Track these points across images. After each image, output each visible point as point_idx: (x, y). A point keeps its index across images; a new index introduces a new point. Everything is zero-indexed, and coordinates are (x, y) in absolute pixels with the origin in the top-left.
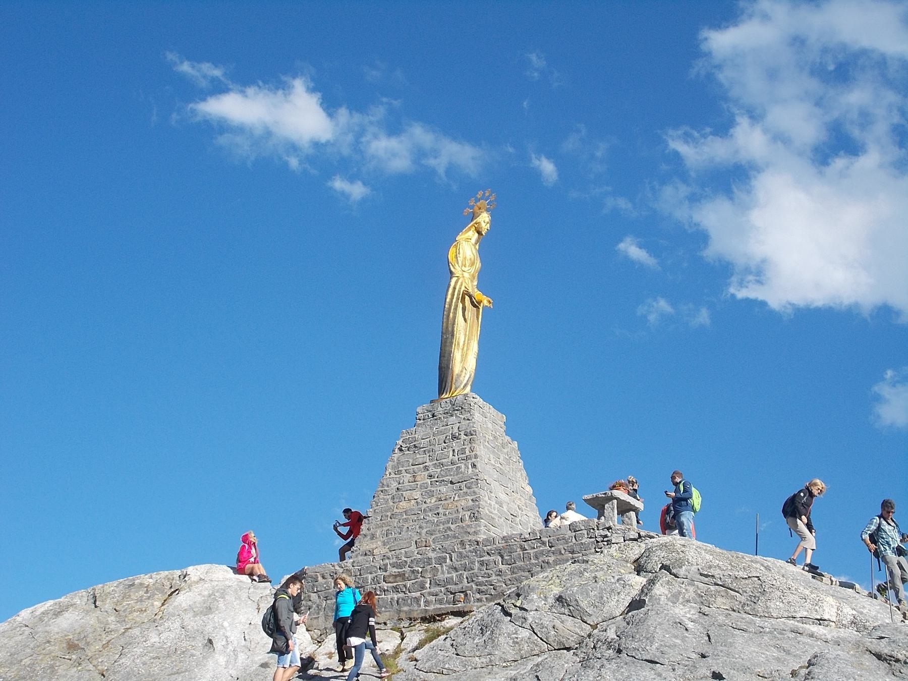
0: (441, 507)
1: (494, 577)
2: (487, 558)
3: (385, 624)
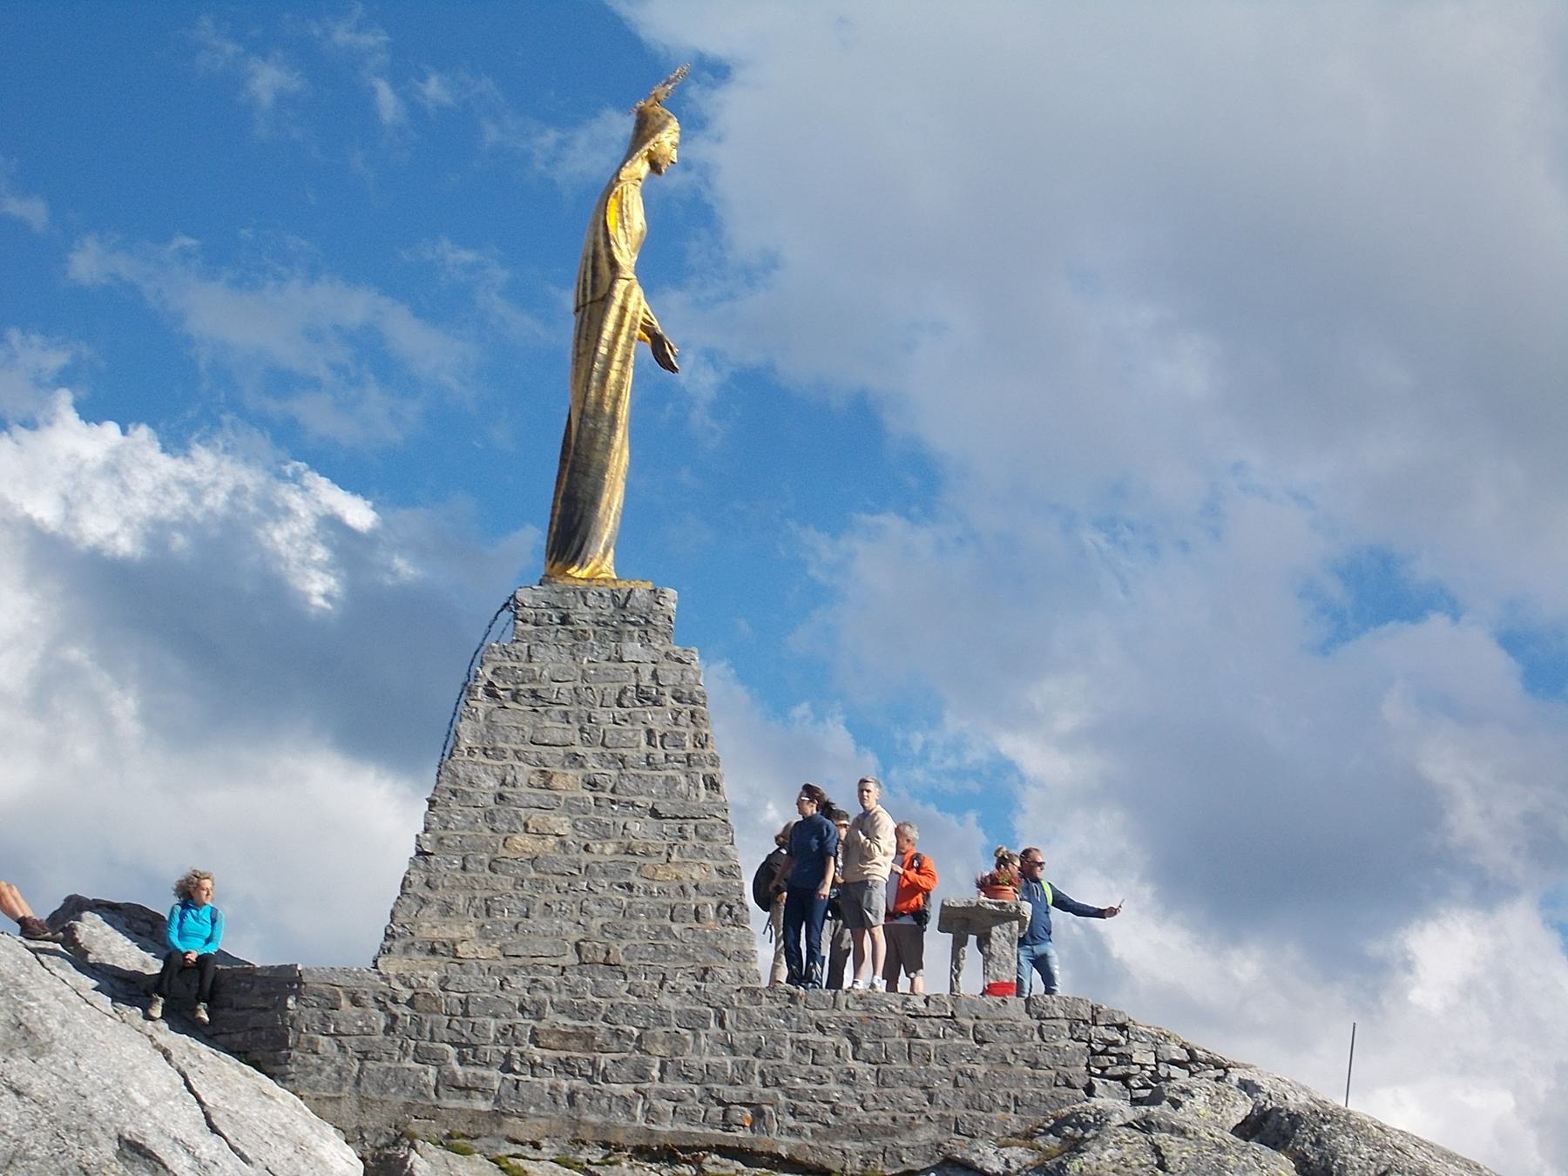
0: (633, 869)
1: (832, 1085)
2: (814, 1037)
3: (536, 1146)
